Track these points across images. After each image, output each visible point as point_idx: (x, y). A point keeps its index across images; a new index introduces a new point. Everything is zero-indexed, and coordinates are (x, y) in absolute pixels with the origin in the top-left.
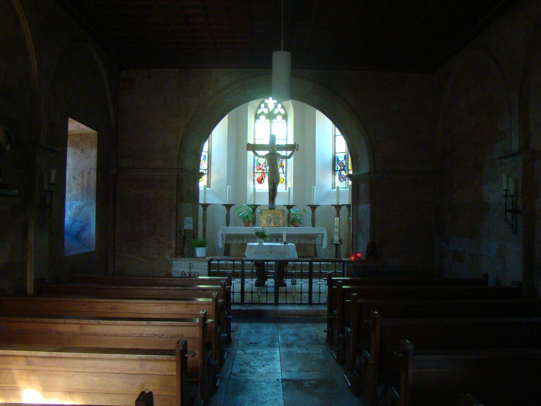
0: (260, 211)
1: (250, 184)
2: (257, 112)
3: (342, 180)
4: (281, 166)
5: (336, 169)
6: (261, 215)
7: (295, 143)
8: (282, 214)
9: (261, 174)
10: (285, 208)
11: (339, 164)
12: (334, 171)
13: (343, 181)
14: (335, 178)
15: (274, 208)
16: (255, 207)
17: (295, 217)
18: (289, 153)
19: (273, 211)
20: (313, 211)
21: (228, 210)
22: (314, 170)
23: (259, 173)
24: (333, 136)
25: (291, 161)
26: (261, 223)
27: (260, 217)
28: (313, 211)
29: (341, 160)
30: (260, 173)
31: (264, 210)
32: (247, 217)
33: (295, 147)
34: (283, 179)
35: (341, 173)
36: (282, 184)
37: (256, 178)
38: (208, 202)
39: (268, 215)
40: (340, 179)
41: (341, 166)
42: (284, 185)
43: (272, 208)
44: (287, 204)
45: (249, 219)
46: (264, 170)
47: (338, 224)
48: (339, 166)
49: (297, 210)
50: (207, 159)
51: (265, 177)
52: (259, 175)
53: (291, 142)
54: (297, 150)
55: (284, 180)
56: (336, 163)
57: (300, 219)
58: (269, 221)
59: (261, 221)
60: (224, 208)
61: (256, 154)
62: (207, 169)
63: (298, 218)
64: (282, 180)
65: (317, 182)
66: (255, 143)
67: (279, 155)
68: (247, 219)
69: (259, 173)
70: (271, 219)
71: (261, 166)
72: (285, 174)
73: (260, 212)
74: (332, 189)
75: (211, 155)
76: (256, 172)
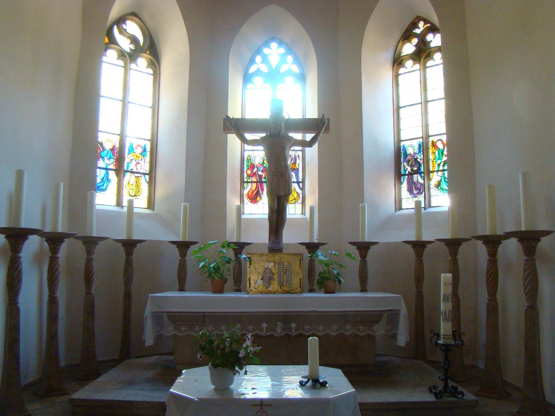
0: (248, 256)
1: (233, 201)
2: (249, 70)
3: (415, 192)
4: (294, 169)
5: (403, 172)
6: (250, 264)
7: (323, 116)
8: (297, 263)
9: (254, 185)
10: (304, 250)
11: (408, 161)
12: (399, 175)
13: (418, 193)
14: (400, 189)
15: (280, 250)
16: (240, 247)
17: (326, 269)
18: (309, 137)
19: (277, 257)
20: (363, 256)
21: (183, 254)
22: (362, 172)
23: (252, 182)
24: (395, 107)
25: (312, 152)
26: (250, 283)
27: (248, 270)
28: (363, 256)
29: (412, 153)
30: (254, 182)
31: (256, 254)
32: (217, 269)
33: (324, 124)
34: (297, 192)
35: (412, 179)
36: (295, 203)
37: (246, 192)
38: (135, 237)
39: (266, 266)
40: (410, 190)
41: (411, 166)
42: (299, 206)
43: (276, 250)
44: (307, 241)
45: (222, 275)
46: (260, 177)
47: (449, 290)
48: (408, 165)
49: (331, 254)
50: (148, 154)
51: (263, 190)
52: (252, 186)
53: (312, 113)
54: (328, 129)
55: (299, 196)
56: (402, 160)
57: (338, 274)
58: (267, 279)
59: (250, 279)
60: (175, 250)
61: (244, 141)
62: (148, 172)
63: (335, 272)
64: (295, 195)
65: (366, 195)
66: (244, 117)
67: (291, 138)
68: (217, 274)
69: (252, 182)
70: (273, 274)
71: (255, 170)
72: (301, 184)
73: (248, 259)
74: (396, 212)
75: (157, 146)
76: (245, 180)
